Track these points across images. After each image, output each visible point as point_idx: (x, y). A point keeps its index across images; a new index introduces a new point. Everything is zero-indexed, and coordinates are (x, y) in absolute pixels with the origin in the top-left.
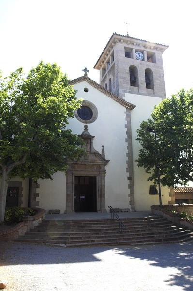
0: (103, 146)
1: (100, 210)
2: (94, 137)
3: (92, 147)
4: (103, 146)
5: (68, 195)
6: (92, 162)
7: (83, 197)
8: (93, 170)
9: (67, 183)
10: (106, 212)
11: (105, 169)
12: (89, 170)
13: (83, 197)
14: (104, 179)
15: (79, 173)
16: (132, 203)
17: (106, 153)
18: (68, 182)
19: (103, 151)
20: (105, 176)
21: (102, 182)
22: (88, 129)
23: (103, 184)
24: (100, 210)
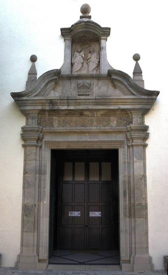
0: (136, 58)
1: (129, 262)
2: (107, 32)
3: (102, 62)
4: (136, 58)
5: (27, 210)
6: (102, 100)
7: (97, 214)
8: (107, 128)
9: (25, 172)
10: (152, 266)
11: (146, 123)
12: (94, 128)
13: (97, 214)
14: (143, 158)
15: (74, 138)
16: (74, 166)
17: (145, 76)
18: (27, 167)
19: (138, 71)
20: (145, 146)
21: (137, 164)
22: (148, 142)
23: (137, 172)
24: (129, 262)
